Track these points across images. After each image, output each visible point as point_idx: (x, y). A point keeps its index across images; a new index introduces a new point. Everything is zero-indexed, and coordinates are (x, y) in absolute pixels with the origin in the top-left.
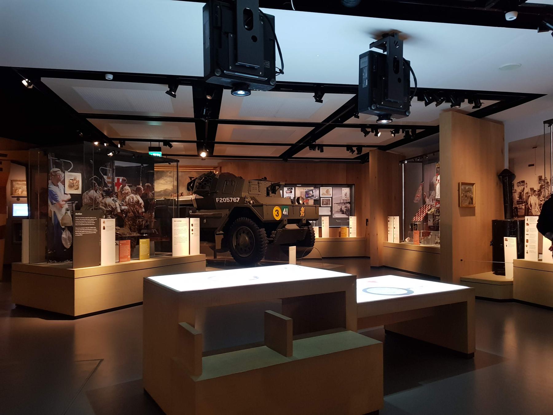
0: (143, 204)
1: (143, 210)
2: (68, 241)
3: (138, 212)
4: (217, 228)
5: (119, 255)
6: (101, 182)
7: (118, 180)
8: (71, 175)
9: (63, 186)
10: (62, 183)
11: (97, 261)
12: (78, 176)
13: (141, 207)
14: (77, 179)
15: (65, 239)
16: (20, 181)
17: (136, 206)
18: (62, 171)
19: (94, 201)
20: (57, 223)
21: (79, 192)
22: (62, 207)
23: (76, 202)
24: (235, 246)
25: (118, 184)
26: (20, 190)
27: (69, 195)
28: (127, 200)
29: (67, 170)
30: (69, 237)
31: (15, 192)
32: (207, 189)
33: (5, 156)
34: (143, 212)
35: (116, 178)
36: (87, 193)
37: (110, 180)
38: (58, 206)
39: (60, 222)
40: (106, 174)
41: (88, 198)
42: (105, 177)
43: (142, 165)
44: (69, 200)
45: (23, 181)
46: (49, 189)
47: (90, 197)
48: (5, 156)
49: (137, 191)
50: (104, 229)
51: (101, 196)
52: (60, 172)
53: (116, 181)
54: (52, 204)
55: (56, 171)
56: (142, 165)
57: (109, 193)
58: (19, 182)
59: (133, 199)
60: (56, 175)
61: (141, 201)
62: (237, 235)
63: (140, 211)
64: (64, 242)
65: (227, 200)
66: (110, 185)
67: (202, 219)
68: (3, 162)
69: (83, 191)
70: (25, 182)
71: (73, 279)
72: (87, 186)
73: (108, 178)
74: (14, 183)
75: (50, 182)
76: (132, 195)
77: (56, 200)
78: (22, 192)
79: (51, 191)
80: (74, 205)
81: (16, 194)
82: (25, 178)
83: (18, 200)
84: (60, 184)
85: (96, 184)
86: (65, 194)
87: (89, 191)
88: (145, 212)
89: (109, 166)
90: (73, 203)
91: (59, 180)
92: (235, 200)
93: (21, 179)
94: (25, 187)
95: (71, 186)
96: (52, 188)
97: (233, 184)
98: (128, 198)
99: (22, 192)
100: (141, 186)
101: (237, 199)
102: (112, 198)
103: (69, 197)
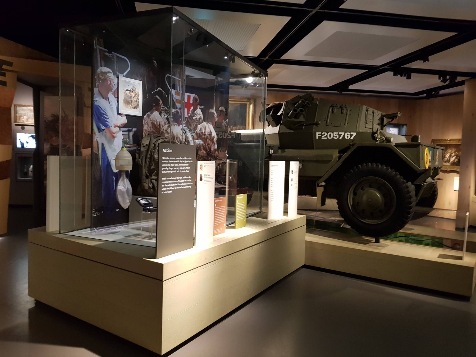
0: (216, 137)
1: (216, 147)
2: (126, 196)
3: (210, 149)
4: (321, 177)
5: (216, 227)
6: (167, 100)
7: (189, 97)
8: (127, 82)
9: (116, 100)
10: (114, 94)
11: (190, 241)
12: (137, 86)
13: (213, 142)
14: (137, 91)
15: (122, 193)
16: (25, 106)
17: (209, 141)
18: (114, 74)
19: (157, 128)
20: (106, 163)
21: (138, 112)
22: (114, 137)
23: (135, 129)
24: (353, 206)
25: (188, 105)
26: (25, 117)
27: (125, 118)
28: (198, 130)
29: (122, 73)
30: (128, 190)
31: (20, 119)
32: (301, 119)
33: (10, 64)
34: (215, 150)
35: (187, 94)
36: (149, 116)
37: (179, 98)
38: (108, 135)
39: (113, 163)
40: (174, 87)
41: (150, 125)
42: (173, 92)
43: (216, 78)
44: (125, 126)
45: (29, 106)
46: (95, 103)
47: (152, 123)
48: (10, 64)
49: (207, 117)
50: (201, 179)
51: (166, 121)
52: (112, 75)
53: (186, 100)
54: (100, 130)
55: (106, 73)
56: (216, 78)
57: (177, 119)
58: (24, 108)
59: (205, 129)
60: (105, 80)
61: (214, 134)
62: (355, 189)
63: (212, 149)
64: (120, 199)
65: (334, 135)
66: (178, 105)
67: (303, 162)
68: (7, 73)
69: (144, 112)
70: (32, 108)
71: (161, 281)
72: (149, 106)
73: (177, 93)
74: (18, 108)
75: (96, 90)
76: (205, 123)
77: (106, 126)
78: (27, 120)
79: (98, 108)
80: (131, 134)
81: (20, 122)
82: (31, 103)
83: (23, 128)
84: (111, 96)
85: (161, 102)
86: (118, 114)
87: (152, 113)
88: (218, 150)
89: (178, 75)
90: (129, 131)
91: (109, 89)
92: (347, 136)
93: (26, 104)
94: (32, 114)
95: (128, 102)
96: (100, 102)
97: (345, 111)
98: (199, 127)
99: (27, 120)
100: (214, 111)
101: (351, 135)
102: (181, 126)
103: (124, 120)
